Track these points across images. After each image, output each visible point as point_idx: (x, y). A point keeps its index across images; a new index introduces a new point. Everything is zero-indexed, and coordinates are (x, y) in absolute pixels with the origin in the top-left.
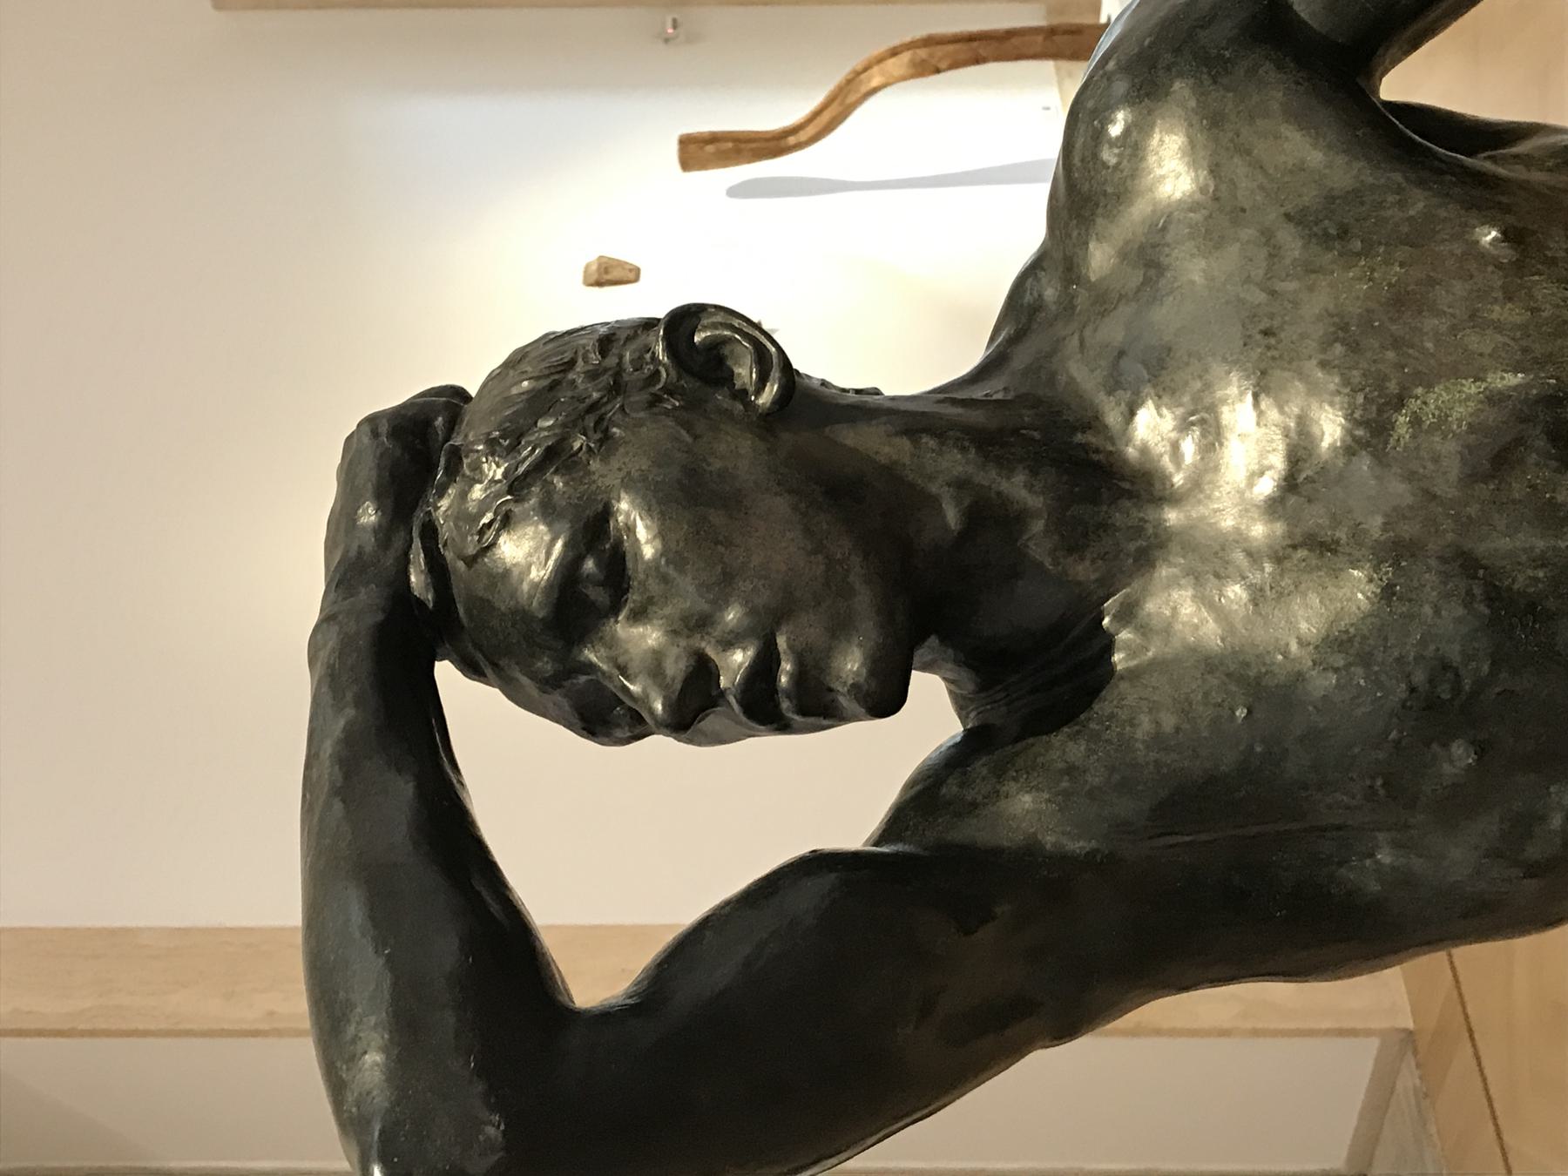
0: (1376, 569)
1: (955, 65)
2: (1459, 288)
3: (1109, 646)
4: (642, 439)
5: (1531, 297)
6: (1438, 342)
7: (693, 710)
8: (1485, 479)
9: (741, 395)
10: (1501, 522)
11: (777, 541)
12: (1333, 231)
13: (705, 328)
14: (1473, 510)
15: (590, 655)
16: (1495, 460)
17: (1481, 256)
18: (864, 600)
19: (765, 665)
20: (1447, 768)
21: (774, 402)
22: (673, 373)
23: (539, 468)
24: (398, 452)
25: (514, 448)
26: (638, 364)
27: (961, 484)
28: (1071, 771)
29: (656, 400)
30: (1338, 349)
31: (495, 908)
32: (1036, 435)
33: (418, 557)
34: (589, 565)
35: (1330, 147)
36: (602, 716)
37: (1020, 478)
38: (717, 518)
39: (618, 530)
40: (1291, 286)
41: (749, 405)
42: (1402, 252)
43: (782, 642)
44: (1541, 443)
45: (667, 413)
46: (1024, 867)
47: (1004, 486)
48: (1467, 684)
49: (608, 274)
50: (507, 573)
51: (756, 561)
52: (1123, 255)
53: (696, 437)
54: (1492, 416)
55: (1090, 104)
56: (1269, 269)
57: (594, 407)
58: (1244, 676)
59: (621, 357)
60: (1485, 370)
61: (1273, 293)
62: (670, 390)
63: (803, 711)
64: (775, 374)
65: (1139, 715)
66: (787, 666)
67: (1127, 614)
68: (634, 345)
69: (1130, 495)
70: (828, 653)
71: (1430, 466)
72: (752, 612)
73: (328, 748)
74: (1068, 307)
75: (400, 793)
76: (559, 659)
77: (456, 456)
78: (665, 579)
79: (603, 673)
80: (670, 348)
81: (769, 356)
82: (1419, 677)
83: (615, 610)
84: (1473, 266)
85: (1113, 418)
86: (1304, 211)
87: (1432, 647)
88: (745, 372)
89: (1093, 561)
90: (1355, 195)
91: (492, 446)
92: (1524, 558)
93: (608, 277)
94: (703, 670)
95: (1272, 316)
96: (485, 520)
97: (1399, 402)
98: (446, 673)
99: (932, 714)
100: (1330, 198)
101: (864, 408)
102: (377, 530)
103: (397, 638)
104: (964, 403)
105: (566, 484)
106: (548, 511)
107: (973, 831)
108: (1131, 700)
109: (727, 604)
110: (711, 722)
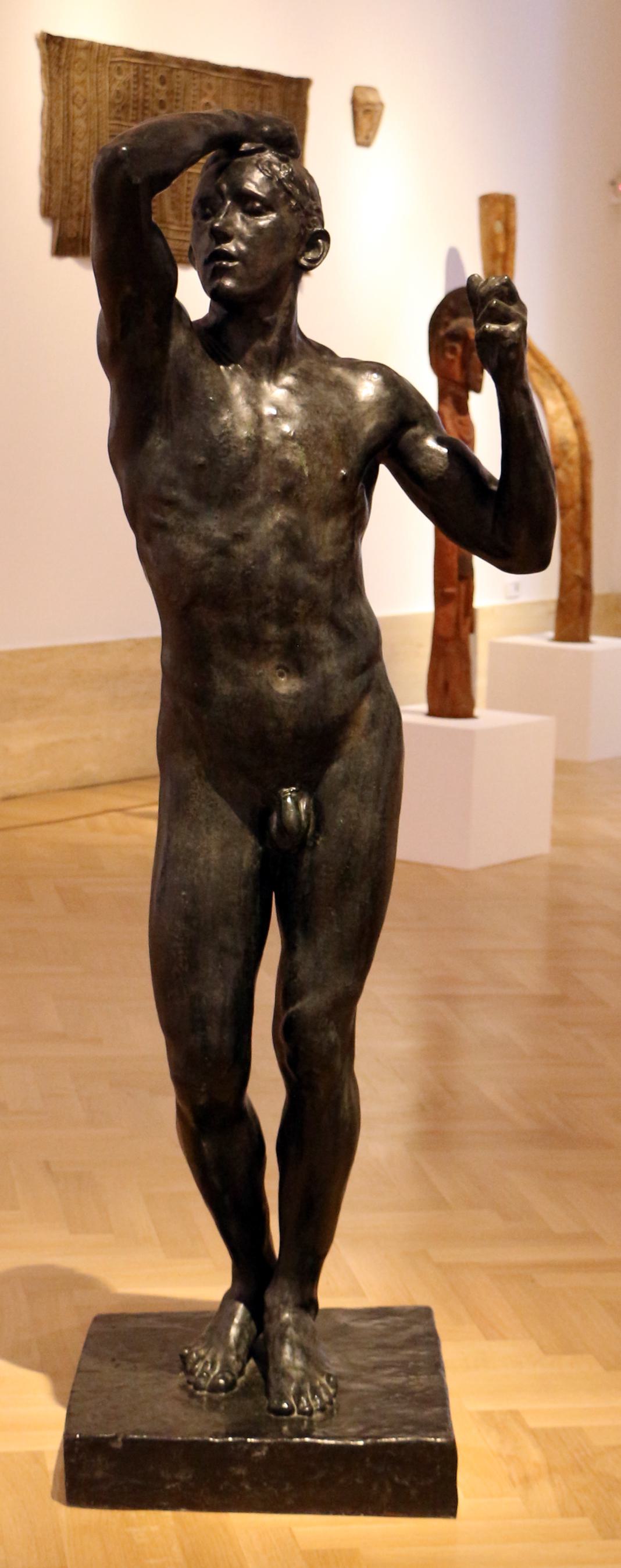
3: (226, 365)
4: (292, 222)
9: (303, 255)
11: (268, 263)
15: (229, 202)
16: (285, 467)
17: (338, 470)
18: (247, 288)
19: (229, 257)
20: (196, 457)
23: (285, 189)
26: (314, 221)
27: (275, 321)
34: (258, 205)
43: (236, 263)
44: (289, 480)
46: (163, 338)
47: (274, 334)
48: (223, 460)
49: (365, 114)
52: (338, 377)
57: (302, 207)
58: (224, 399)
67: (236, 370)
74: (324, 362)
80: (318, 232)
81: (314, 263)
82: (226, 446)
85: (293, 370)
88: (310, 255)
90: (355, 439)
91: (291, 174)
93: (360, 114)
94: (228, 238)
97: (301, 444)
100: (356, 432)
101: (292, 309)
102: (262, 133)
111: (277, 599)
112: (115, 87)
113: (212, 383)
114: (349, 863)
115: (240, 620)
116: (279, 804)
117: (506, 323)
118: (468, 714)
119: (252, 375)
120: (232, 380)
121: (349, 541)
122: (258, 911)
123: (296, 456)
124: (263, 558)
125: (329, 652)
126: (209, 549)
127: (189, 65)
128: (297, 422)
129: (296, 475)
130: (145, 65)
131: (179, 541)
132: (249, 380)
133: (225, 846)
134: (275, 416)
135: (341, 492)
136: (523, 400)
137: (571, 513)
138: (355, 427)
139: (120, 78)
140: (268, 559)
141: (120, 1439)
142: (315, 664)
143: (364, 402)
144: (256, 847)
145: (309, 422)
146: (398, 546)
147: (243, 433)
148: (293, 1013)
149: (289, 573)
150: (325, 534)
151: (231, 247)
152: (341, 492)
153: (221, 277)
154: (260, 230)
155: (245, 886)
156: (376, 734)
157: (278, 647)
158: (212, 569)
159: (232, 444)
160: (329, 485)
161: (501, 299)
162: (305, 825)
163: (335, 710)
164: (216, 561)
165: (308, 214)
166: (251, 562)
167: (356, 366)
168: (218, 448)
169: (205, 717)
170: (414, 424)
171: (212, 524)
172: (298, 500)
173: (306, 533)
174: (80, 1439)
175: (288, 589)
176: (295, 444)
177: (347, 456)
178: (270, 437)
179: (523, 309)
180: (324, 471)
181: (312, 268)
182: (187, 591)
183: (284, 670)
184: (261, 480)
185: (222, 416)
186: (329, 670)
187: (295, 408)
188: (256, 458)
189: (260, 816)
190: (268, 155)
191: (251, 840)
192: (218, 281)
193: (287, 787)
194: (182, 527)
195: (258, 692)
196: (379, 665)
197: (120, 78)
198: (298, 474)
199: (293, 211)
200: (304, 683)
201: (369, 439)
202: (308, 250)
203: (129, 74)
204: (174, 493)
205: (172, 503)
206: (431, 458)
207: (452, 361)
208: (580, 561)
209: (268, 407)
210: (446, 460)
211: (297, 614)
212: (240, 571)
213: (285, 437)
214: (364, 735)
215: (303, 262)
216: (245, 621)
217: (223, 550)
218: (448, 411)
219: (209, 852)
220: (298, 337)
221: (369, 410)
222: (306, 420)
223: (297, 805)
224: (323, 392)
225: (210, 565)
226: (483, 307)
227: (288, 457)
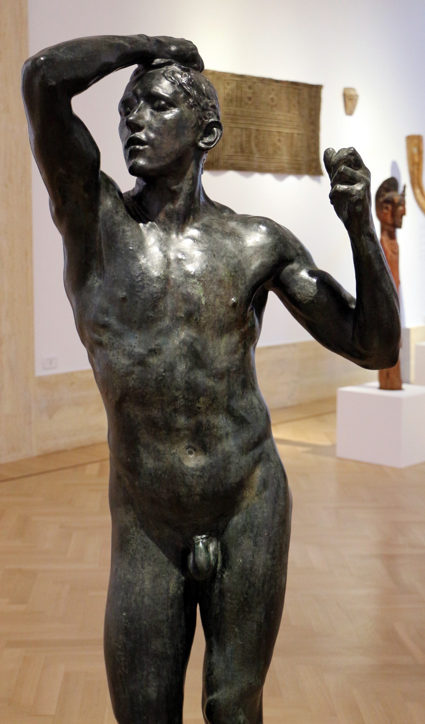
0: (163, 275)
2: (223, 293)
3: (145, 222)
4: (192, 115)
5: (221, 307)
6: (212, 288)
7: (134, 127)
8: (183, 298)
9: (202, 139)
10: (173, 301)
11: (171, 146)
12: (236, 269)
13: (217, 131)
14: (176, 295)
15: (142, 102)
16: (187, 299)
18: (156, 165)
19: (141, 142)
21: (200, 146)
22: (207, 123)
23: (185, 91)
24: (188, 56)
26: (209, 115)
27: (181, 189)
29: (201, 119)
30: (210, 269)
31: (91, 83)
32: (192, 207)
34: (163, 103)
35: (255, 270)
36: (127, 105)
38: (174, 132)
39: (171, 110)
40: (224, 261)
41: (199, 140)
43: (146, 147)
45: (197, 121)
46: (94, 204)
47: (181, 199)
48: (139, 294)
49: (349, 100)
50: (160, 83)
51: (165, 141)
52: (233, 229)
53: (192, 128)
54: (196, 298)
55: (268, 221)
56: (228, 257)
57: (199, 104)
59: (210, 110)
60: (206, 297)
62: (203, 122)
63: (131, 152)
64: (206, 146)
65: (128, 229)
66: (141, 148)
67: (152, 227)
68: (213, 113)
69: (179, 227)
71: (185, 286)
72: (153, 140)
73: (122, 42)
74: (223, 218)
75: (112, 59)
76: (139, 95)
77: (188, 71)
78: (160, 120)
79: (138, 106)
80: (212, 122)
82: (140, 284)
83: (153, 108)
84: (227, 296)
85: (196, 225)
86: (241, 264)
87: (147, 286)
89: (164, 219)
90: (244, 275)
91: (189, 80)
92: (166, 305)
94: (140, 128)
95: (218, 257)
96: (173, 78)
97: (199, 280)
98: (136, 66)
99: (127, 183)
100: (244, 270)
102: (170, 51)
103: (145, 56)
104: (199, 192)
105: (181, 97)
106: (175, 93)
107: (103, 191)
108: (133, 226)
109: (155, 134)
110: (126, 131)
111: (183, 398)
112: (226, 91)
113: (132, 237)
114: (247, 594)
115: (156, 413)
118: (399, 388)
119: (164, 230)
120: (148, 235)
122: (183, 624)
123: (197, 291)
125: (227, 434)
126: (132, 361)
127: (263, 80)
129: (195, 304)
130: (241, 81)
131: (111, 354)
132: (161, 234)
133: (156, 577)
135: (232, 315)
136: (371, 243)
139: (229, 87)
142: (216, 445)
143: (251, 247)
144: (180, 577)
147: (155, 273)
148: (211, 700)
149: (192, 377)
152: (232, 315)
154: (165, 122)
155: (172, 606)
156: (266, 494)
157: (187, 432)
158: (134, 376)
159: (145, 282)
160: (222, 310)
161: (349, 166)
162: (213, 563)
163: (233, 478)
164: (137, 369)
165: (204, 110)
166: (162, 370)
167: (248, 221)
168: (135, 283)
169: (137, 483)
170: (291, 261)
171: (133, 342)
172: (198, 323)
173: (204, 348)
175: (193, 389)
176: (195, 280)
177: (236, 287)
179: (367, 173)
180: (218, 300)
182: (118, 391)
183: (192, 449)
184: (169, 309)
186: (227, 449)
188: (164, 292)
189: (181, 555)
190: (175, 67)
191: (176, 572)
192: (133, 160)
193: (200, 535)
194: (113, 344)
195: (172, 467)
197: (229, 87)
198: (198, 305)
199: (191, 107)
200: (207, 459)
201: (255, 275)
202: (206, 136)
203: (233, 85)
204: (107, 319)
205: (105, 326)
206: (304, 287)
207: (387, 214)
209: (172, 253)
210: (315, 288)
211: (199, 408)
212: (154, 377)
213: (187, 275)
214: (257, 495)
215: (201, 144)
216: (160, 415)
217: (141, 362)
218: (386, 238)
219: (144, 582)
221: (255, 253)
222: (205, 262)
223: (206, 548)
224: (220, 241)
226: (335, 172)
227: (189, 290)
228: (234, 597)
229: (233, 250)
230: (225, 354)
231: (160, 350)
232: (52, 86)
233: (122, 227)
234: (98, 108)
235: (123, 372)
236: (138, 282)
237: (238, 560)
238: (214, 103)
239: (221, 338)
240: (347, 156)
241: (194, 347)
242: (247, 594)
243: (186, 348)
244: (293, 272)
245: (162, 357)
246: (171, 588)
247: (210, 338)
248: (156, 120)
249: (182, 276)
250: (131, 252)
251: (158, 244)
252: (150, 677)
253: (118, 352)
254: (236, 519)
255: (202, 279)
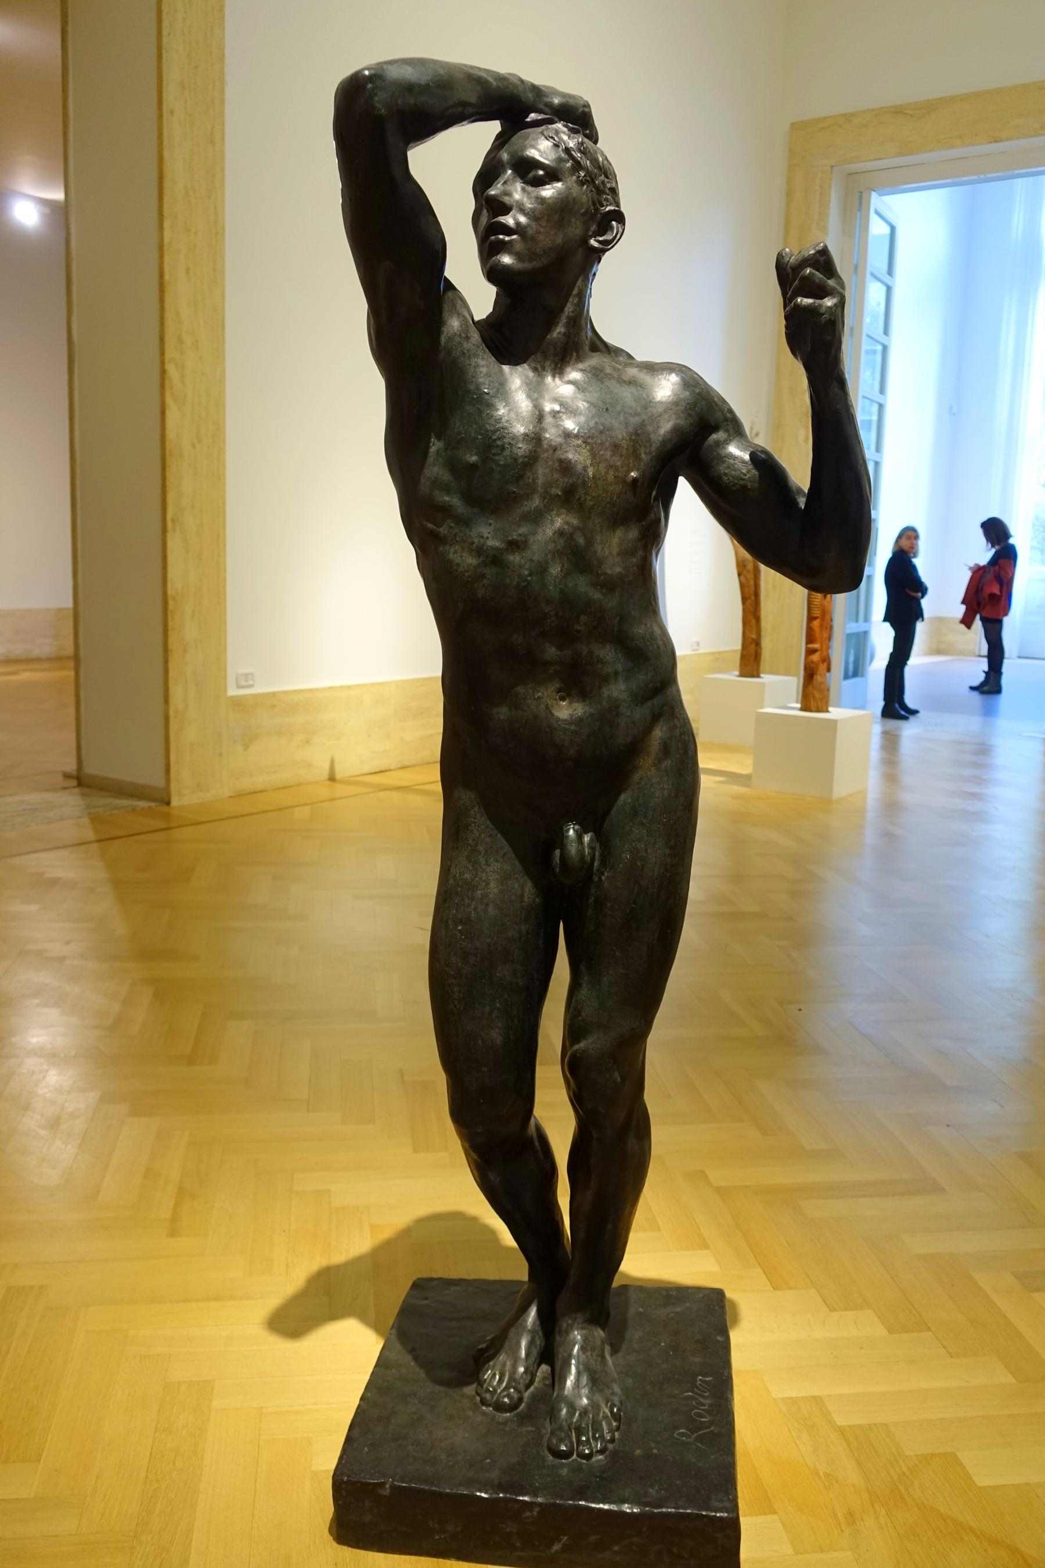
1: (742, 586)
2: (619, 463)
4: (583, 194)
10: (546, 471)
11: (550, 239)
15: (510, 172)
16: (565, 467)
18: (527, 266)
19: (507, 230)
25: (580, 151)
26: (606, 200)
28: (468, 338)
33: (540, 117)
34: (541, 172)
37: (563, 330)
38: (556, 217)
40: (622, 418)
42: (631, 450)
43: (514, 237)
54: (579, 467)
57: (593, 181)
61: (619, 413)
62: (596, 210)
66: (507, 238)
70: (510, 253)
72: (525, 227)
73: (484, 75)
81: (607, 245)
82: (499, 443)
84: (625, 469)
85: (580, 366)
94: (506, 210)
103: (510, 106)
106: (560, 160)
113: (488, 375)
114: (635, 903)
115: (517, 639)
116: (560, 839)
117: (822, 298)
120: (511, 374)
121: (641, 553)
122: (542, 946)
124: (542, 569)
125: (616, 673)
126: (482, 559)
128: (582, 419)
131: (452, 550)
132: (531, 374)
134: (558, 412)
136: (837, 390)
137: (749, 601)
138: (650, 429)
140: (546, 570)
141: (388, 1486)
142: (600, 688)
143: (660, 402)
145: (596, 419)
146: (694, 557)
147: (520, 429)
150: (611, 547)
151: (509, 220)
153: (498, 254)
154: (542, 200)
156: (667, 763)
158: (485, 581)
160: (617, 488)
164: (490, 572)
167: (652, 368)
168: (492, 441)
170: (716, 429)
172: (581, 505)
173: (590, 542)
174: (348, 1482)
177: (637, 456)
178: (551, 435)
179: (842, 285)
181: (604, 251)
185: (497, 410)
186: (615, 694)
187: (582, 405)
188: (532, 459)
189: (538, 854)
196: (674, 689)
200: (587, 708)
201: (664, 442)
204: (447, 498)
208: (754, 629)
211: (578, 631)
212: (515, 583)
213: (567, 435)
214: (655, 765)
215: (593, 242)
217: (495, 560)
219: (488, 884)
220: (589, 333)
222: (593, 417)
225: (483, 576)
227: (570, 456)
228: (616, 907)
229: (634, 404)
230: (618, 554)
231: (526, 542)
232: (378, 125)
233: (473, 360)
234: (446, 167)
235: (469, 576)
236: (495, 440)
237: (624, 856)
238: (614, 185)
239: (614, 531)
240: (814, 255)
241: (574, 540)
242: (635, 903)
243: (562, 541)
244: (718, 444)
245: (528, 554)
246: (526, 895)
247: (598, 529)
248: (529, 198)
249: (560, 436)
250: (487, 397)
251: (524, 387)
252: (495, 1013)
253: (463, 549)
254: (623, 797)
255: (590, 440)
